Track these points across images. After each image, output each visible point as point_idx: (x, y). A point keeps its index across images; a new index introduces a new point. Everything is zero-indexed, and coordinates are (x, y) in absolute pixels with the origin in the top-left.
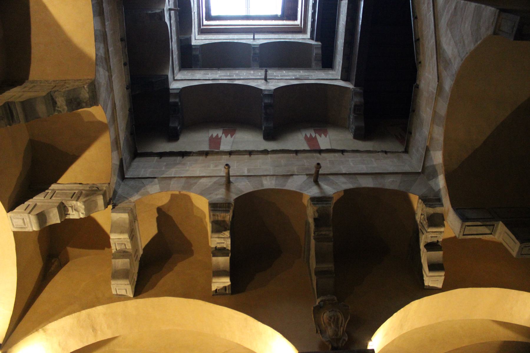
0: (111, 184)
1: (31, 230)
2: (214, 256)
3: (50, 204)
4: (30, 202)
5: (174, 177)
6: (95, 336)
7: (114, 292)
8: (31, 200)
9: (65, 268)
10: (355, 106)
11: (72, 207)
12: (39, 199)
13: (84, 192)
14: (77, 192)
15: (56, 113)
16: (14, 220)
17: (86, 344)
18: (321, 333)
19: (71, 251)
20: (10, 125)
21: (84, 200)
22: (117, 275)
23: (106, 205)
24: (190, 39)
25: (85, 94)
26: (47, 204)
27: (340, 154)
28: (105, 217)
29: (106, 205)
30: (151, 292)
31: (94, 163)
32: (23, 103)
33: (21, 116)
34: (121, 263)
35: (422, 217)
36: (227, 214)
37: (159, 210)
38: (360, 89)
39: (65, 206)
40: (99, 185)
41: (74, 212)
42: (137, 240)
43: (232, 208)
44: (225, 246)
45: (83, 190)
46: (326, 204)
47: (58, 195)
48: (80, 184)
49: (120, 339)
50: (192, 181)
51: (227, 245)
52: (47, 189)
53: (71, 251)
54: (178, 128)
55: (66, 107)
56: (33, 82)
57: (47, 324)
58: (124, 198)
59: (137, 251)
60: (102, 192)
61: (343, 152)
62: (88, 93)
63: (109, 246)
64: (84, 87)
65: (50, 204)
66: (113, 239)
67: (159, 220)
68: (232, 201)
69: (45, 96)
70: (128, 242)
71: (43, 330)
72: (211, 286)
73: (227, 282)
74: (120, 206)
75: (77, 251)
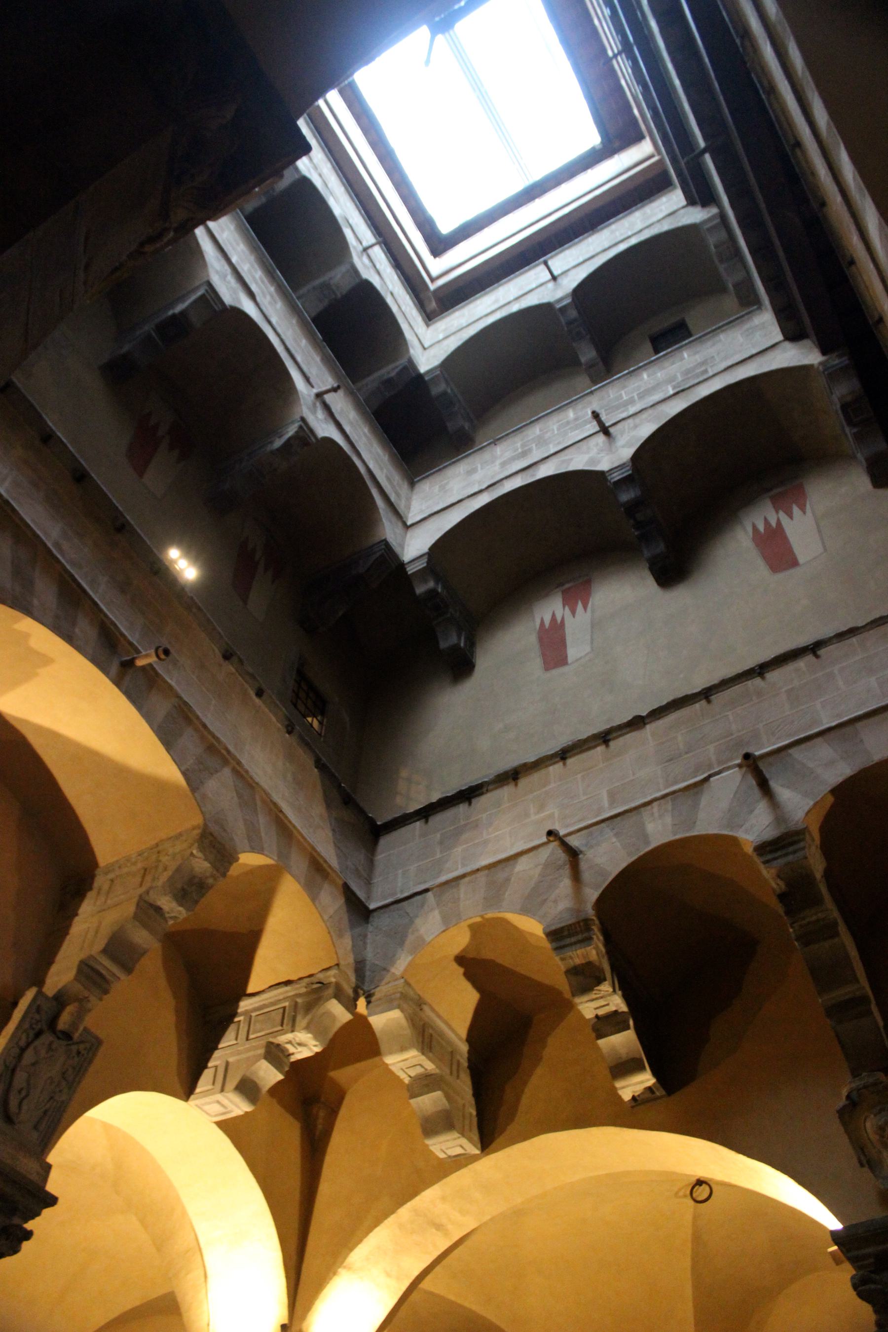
0: (342, 962)
1: (240, 1113)
2: (600, 1036)
3: (251, 1053)
4: (216, 1060)
5: (463, 876)
6: (446, 1233)
9: (343, 1112)
10: (845, 407)
12: (231, 1049)
13: (299, 1000)
14: (286, 1004)
18: (872, 1168)
24: (411, 365)
25: (201, 865)
26: (244, 1056)
27: (810, 658)
30: (512, 1129)
31: (293, 939)
32: (105, 951)
33: (115, 969)
34: (430, 1102)
36: (588, 948)
37: (460, 960)
38: (840, 356)
39: (278, 1045)
40: (321, 976)
41: (300, 1049)
43: (595, 929)
44: (614, 1009)
46: (795, 852)
50: (500, 875)
51: (617, 1005)
52: (235, 1014)
54: (462, 645)
55: (181, 909)
57: (348, 1254)
60: (331, 991)
61: (814, 649)
62: (206, 860)
64: (192, 854)
66: (394, 1064)
67: (468, 976)
68: (590, 912)
71: (345, 1267)
72: (620, 1097)
73: (648, 1080)
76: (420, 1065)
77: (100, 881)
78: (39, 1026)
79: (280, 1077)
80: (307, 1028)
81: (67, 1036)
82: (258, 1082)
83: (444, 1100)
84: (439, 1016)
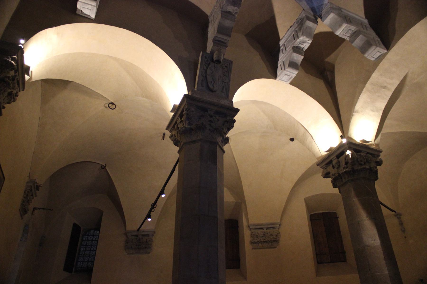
0: (305, 9)
3: (289, 54)
4: (280, 63)
6: (389, 89)
7: (373, 59)
8: (279, 62)
11: (300, 43)
12: (282, 57)
13: (297, 29)
15: (236, 16)
16: (283, 79)
17: (388, 98)
19: (329, 59)
20: (227, 47)
21: (301, 33)
22: (364, 49)
23: (316, 22)
26: (287, 56)
28: (323, 26)
29: (316, 22)
32: (218, 32)
34: (359, 41)
35: (95, 249)
39: (297, 47)
40: (300, 17)
41: (305, 44)
42: (354, 18)
45: (295, 29)
47: (288, 45)
48: (291, 27)
49: (410, 75)
52: (280, 47)
53: (329, 59)
55: (236, 8)
56: (211, 14)
58: (321, 7)
59: (362, 24)
60: (305, 19)
63: (344, 40)
65: (289, 54)
66: (340, 34)
69: (222, 16)
70: (349, 27)
71: (355, 112)
74: (323, 13)
75: (332, 56)
76: (350, 29)
77: (211, 19)
78: (208, 62)
79: (303, 57)
80: (303, 34)
81: (218, 62)
82: (296, 62)
83: (364, 37)
84: (349, 11)
